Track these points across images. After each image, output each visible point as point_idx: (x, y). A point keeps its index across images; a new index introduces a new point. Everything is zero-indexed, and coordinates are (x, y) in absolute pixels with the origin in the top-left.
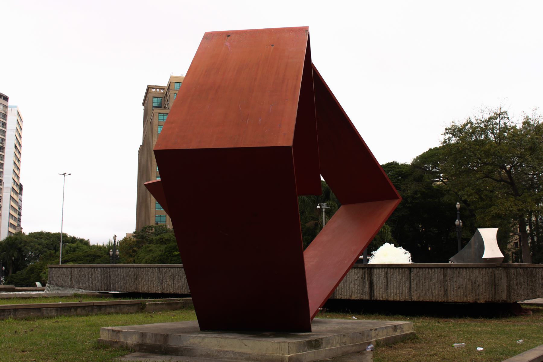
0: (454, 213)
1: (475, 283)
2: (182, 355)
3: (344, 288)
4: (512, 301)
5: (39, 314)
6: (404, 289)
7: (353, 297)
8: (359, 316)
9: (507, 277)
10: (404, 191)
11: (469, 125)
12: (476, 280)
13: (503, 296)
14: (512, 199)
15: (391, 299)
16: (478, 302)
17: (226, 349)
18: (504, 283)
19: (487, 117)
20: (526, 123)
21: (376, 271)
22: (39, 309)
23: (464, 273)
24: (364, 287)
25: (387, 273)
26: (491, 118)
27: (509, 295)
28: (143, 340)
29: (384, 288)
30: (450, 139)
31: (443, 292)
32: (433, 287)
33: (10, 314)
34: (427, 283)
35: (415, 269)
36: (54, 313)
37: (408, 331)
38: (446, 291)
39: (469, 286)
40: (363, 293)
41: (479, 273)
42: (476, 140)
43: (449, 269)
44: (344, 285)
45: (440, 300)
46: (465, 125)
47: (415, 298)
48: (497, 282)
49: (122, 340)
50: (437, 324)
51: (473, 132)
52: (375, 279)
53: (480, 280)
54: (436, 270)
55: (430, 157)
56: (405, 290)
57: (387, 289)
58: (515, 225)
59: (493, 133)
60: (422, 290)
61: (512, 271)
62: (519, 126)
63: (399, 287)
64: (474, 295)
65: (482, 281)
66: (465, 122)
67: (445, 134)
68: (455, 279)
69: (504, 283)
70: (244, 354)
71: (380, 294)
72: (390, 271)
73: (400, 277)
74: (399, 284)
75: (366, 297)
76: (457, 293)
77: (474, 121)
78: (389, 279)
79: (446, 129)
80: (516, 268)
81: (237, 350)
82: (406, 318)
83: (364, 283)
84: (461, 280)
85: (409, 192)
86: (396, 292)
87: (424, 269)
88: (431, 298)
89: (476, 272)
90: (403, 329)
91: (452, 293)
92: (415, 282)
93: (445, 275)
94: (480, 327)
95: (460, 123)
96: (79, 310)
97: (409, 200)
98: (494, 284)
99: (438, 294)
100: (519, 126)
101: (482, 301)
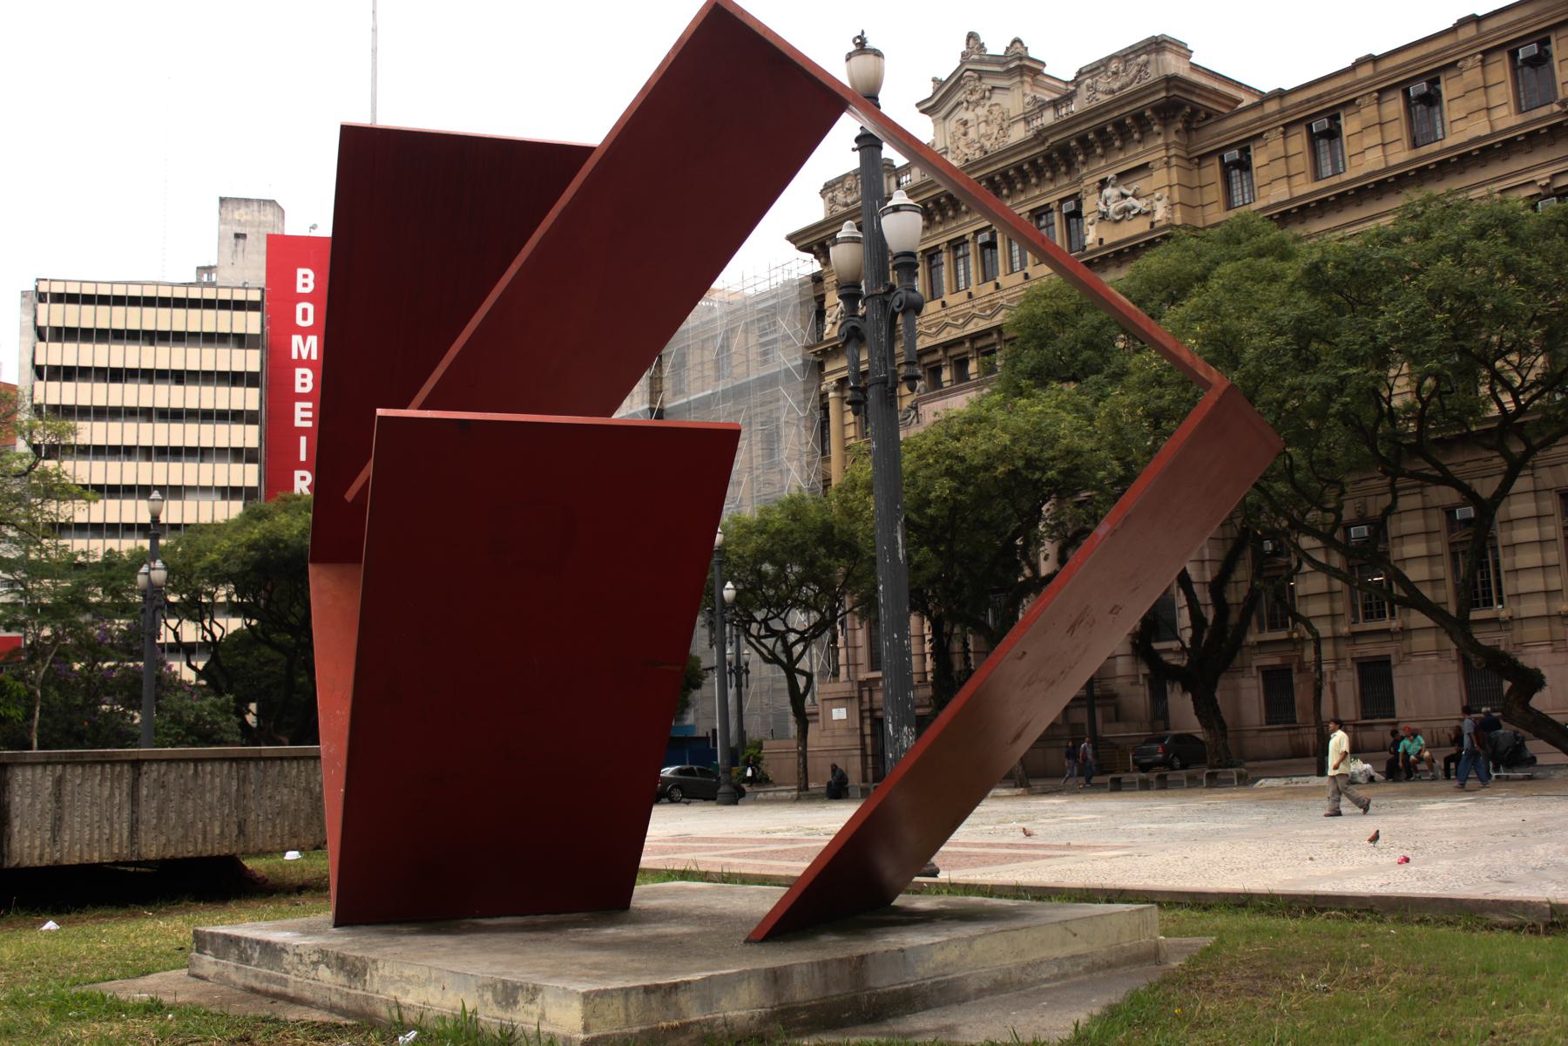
2: (927, 1008)
17: (1030, 958)
23: (294, 772)
28: (779, 996)
32: (207, 814)
34: (190, 803)
35: (155, 766)
43: (252, 765)
49: (695, 1016)
58: (782, 636)
70: (1081, 956)
73: (106, 793)
81: (1059, 953)
84: (286, 791)
93: (243, 780)
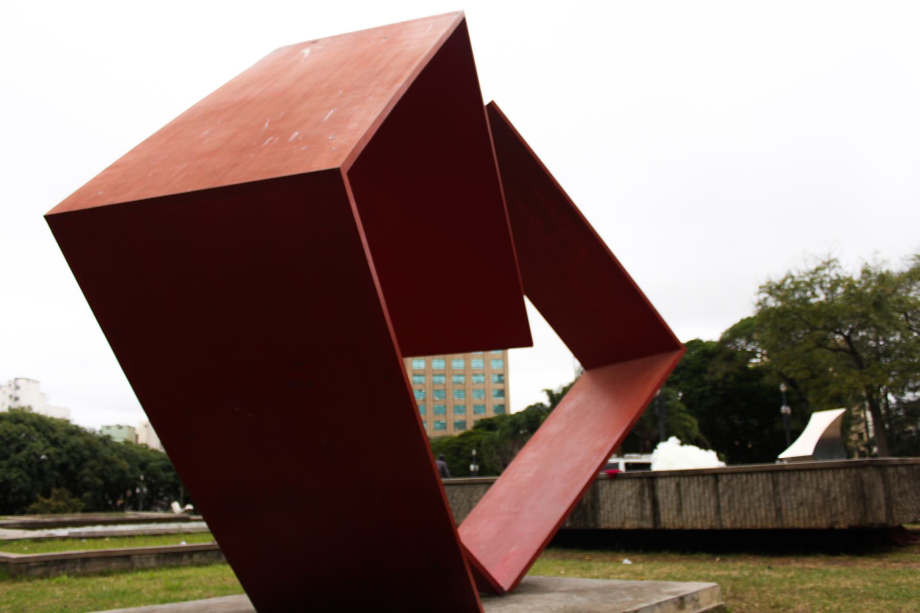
0: (779, 399)
1: (828, 495)
3: (612, 512)
4: (896, 524)
5: (127, 565)
6: (708, 510)
7: (628, 526)
8: (637, 557)
9: (884, 482)
10: (713, 373)
11: (789, 281)
12: (829, 490)
13: (881, 516)
14: (856, 372)
15: (689, 526)
16: (837, 527)
18: (879, 494)
19: (813, 267)
20: (866, 272)
21: (661, 483)
22: (126, 557)
24: (643, 509)
25: (678, 485)
26: (817, 269)
27: (889, 514)
29: (675, 509)
30: (765, 299)
31: (773, 513)
33: (75, 567)
36: (153, 562)
37: (710, 603)
38: (778, 510)
39: (819, 501)
40: (642, 518)
41: (834, 478)
42: (801, 298)
44: (612, 505)
45: (770, 526)
46: (784, 281)
47: (727, 524)
48: (867, 492)
50: (767, 572)
51: (796, 288)
52: (661, 494)
53: (836, 490)
54: (760, 476)
55: (742, 330)
56: (711, 511)
57: (680, 509)
59: (822, 288)
60: (739, 511)
61: (891, 471)
62: (857, 276)
63: (700, 506)
64: (828, 515)
65: (840, 492)
66: (782, 276)
67: (760, 292)
68: (793, 490)
69: (879, 494)
71: (669, 519)
72: (684, 482)
73: (701, 491)
74: (700, 501)
75: (647, 525)
76: (798, 513)
77: (795, 274)
78: (683, 494)
79: (761, 287)
80: (895, 466)
82: (714, 559)
83: (643, 502)
85: (719, 375)
86: (696, 514)
87: (739, 476)
88: (754, 523)
89: (829, 476)
90: (697, 600)
91: (790, 513)
92: (726, 498)
93: (775, 484)
94: (847, 577)
95: (776, 279)
96: (196, 557)
97: (720, 385)
98: (861, 496)
99: (766, 516)
100: (857, 276)
101: (843, 526)
